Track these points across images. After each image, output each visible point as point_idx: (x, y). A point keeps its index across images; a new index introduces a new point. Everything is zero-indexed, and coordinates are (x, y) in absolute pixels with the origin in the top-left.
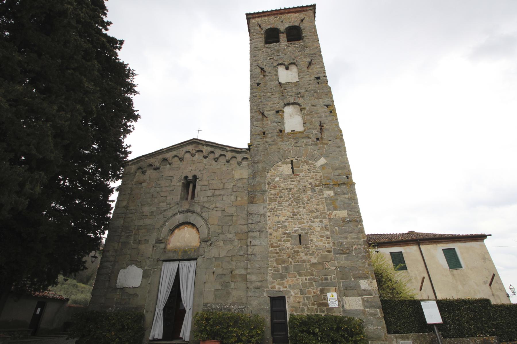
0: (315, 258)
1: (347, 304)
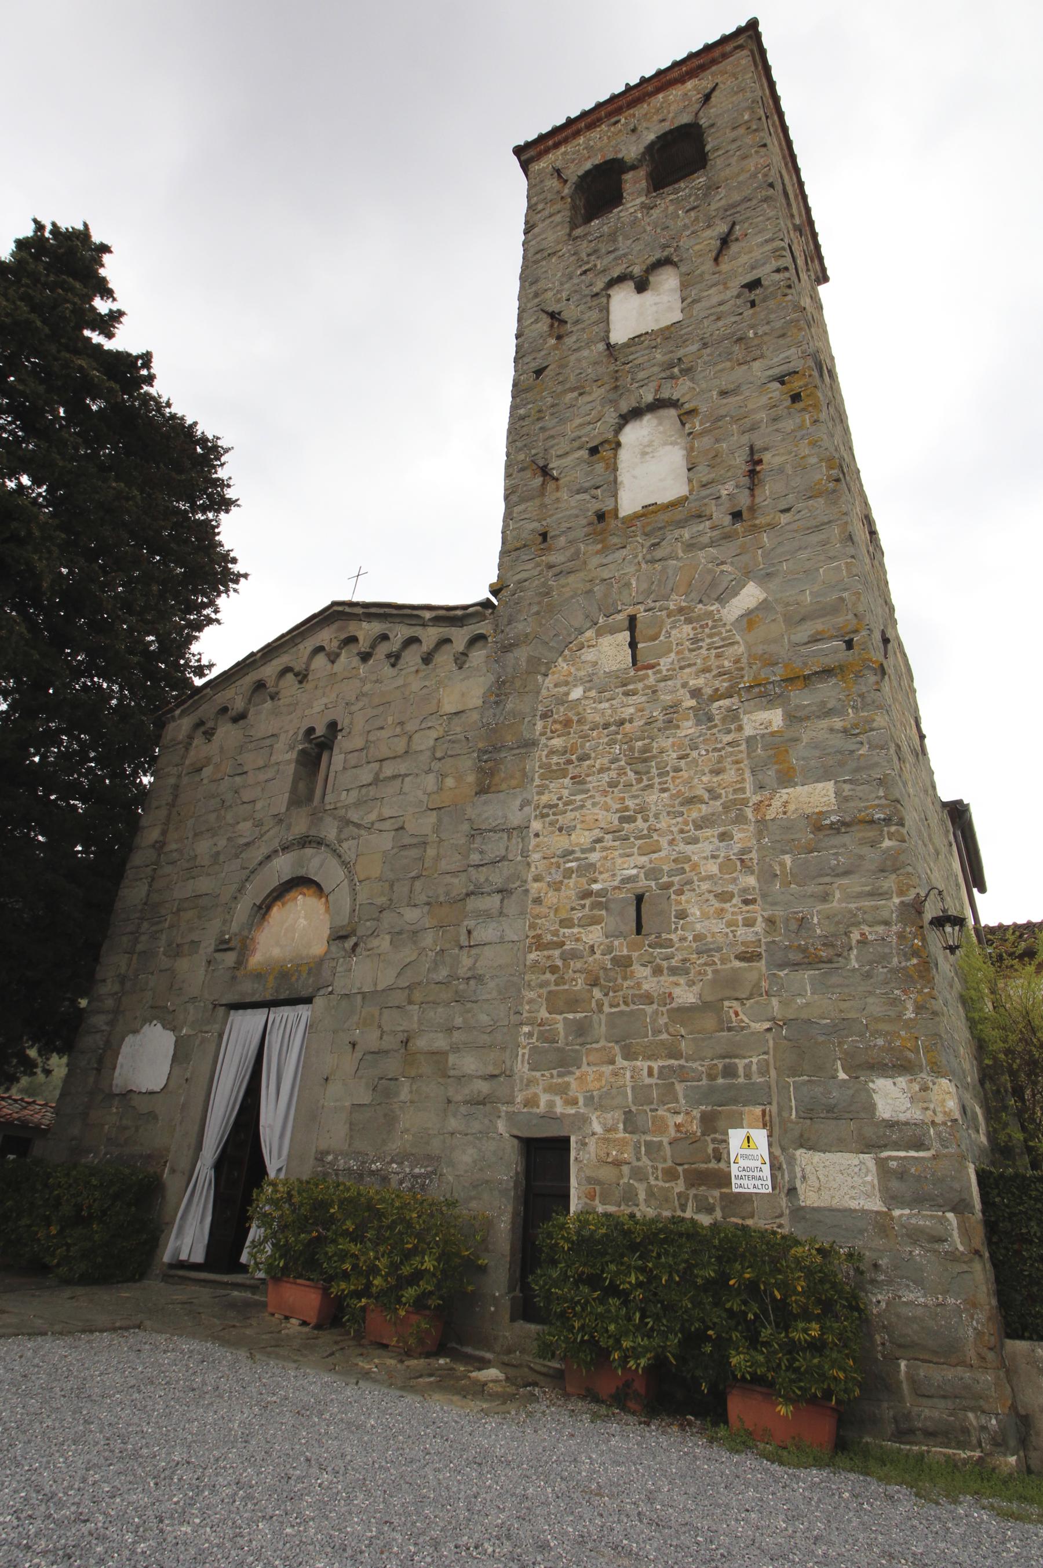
0: (691, 983)
1: (812, 1180)
